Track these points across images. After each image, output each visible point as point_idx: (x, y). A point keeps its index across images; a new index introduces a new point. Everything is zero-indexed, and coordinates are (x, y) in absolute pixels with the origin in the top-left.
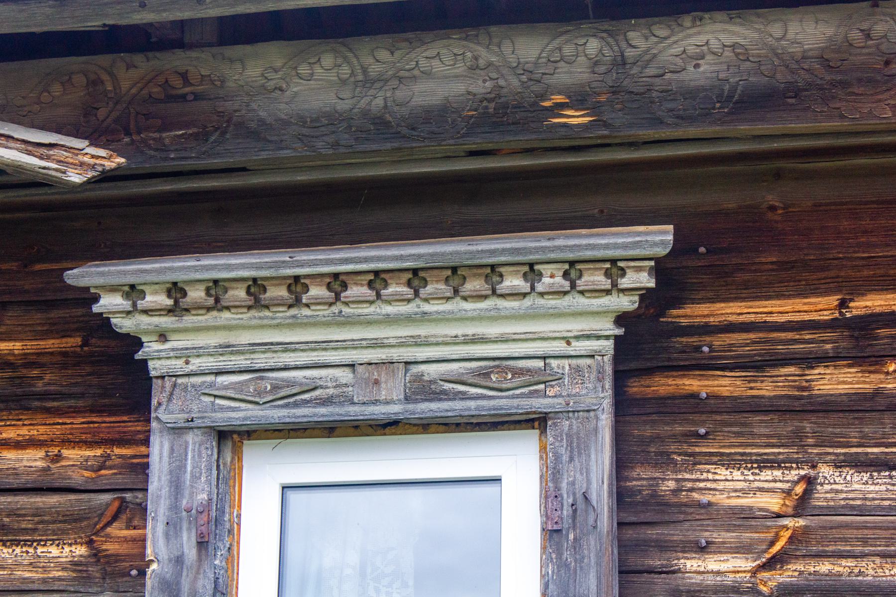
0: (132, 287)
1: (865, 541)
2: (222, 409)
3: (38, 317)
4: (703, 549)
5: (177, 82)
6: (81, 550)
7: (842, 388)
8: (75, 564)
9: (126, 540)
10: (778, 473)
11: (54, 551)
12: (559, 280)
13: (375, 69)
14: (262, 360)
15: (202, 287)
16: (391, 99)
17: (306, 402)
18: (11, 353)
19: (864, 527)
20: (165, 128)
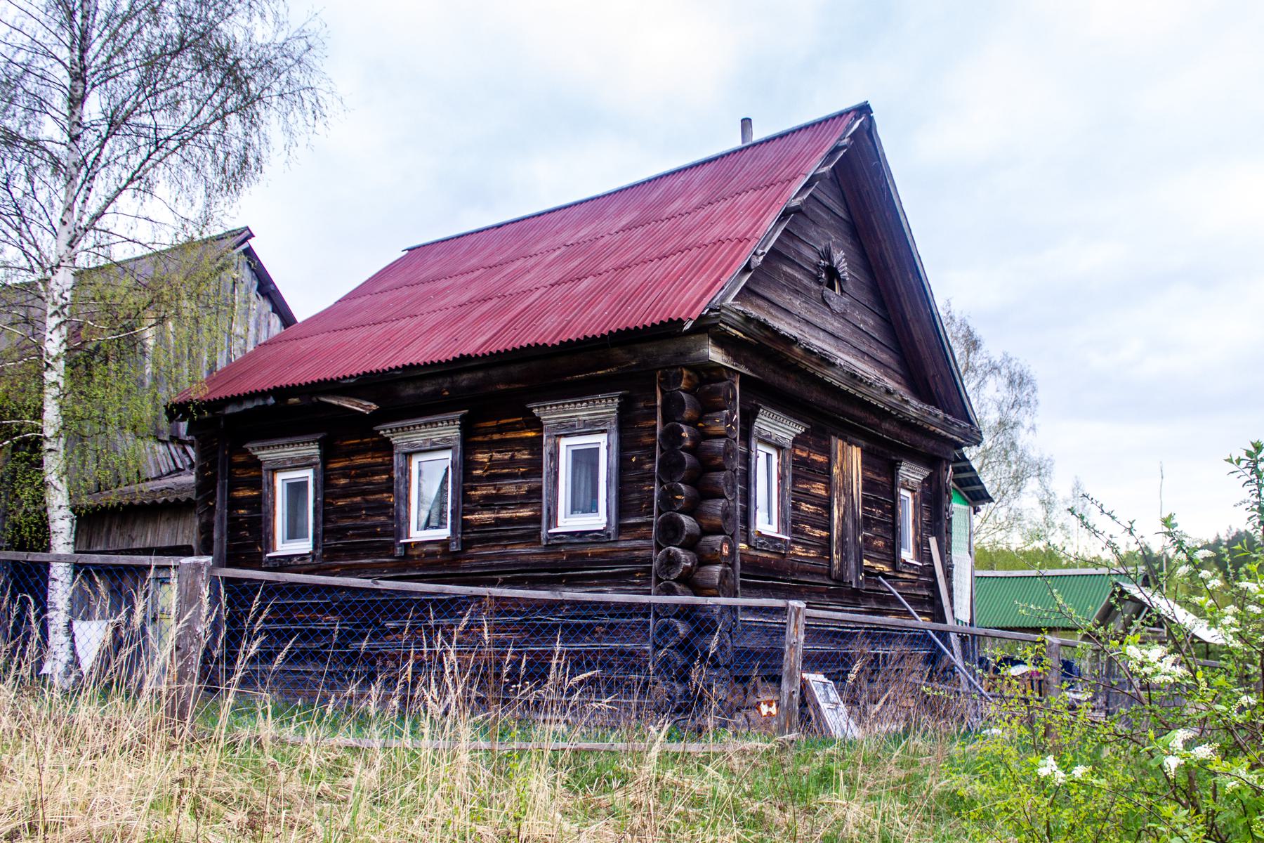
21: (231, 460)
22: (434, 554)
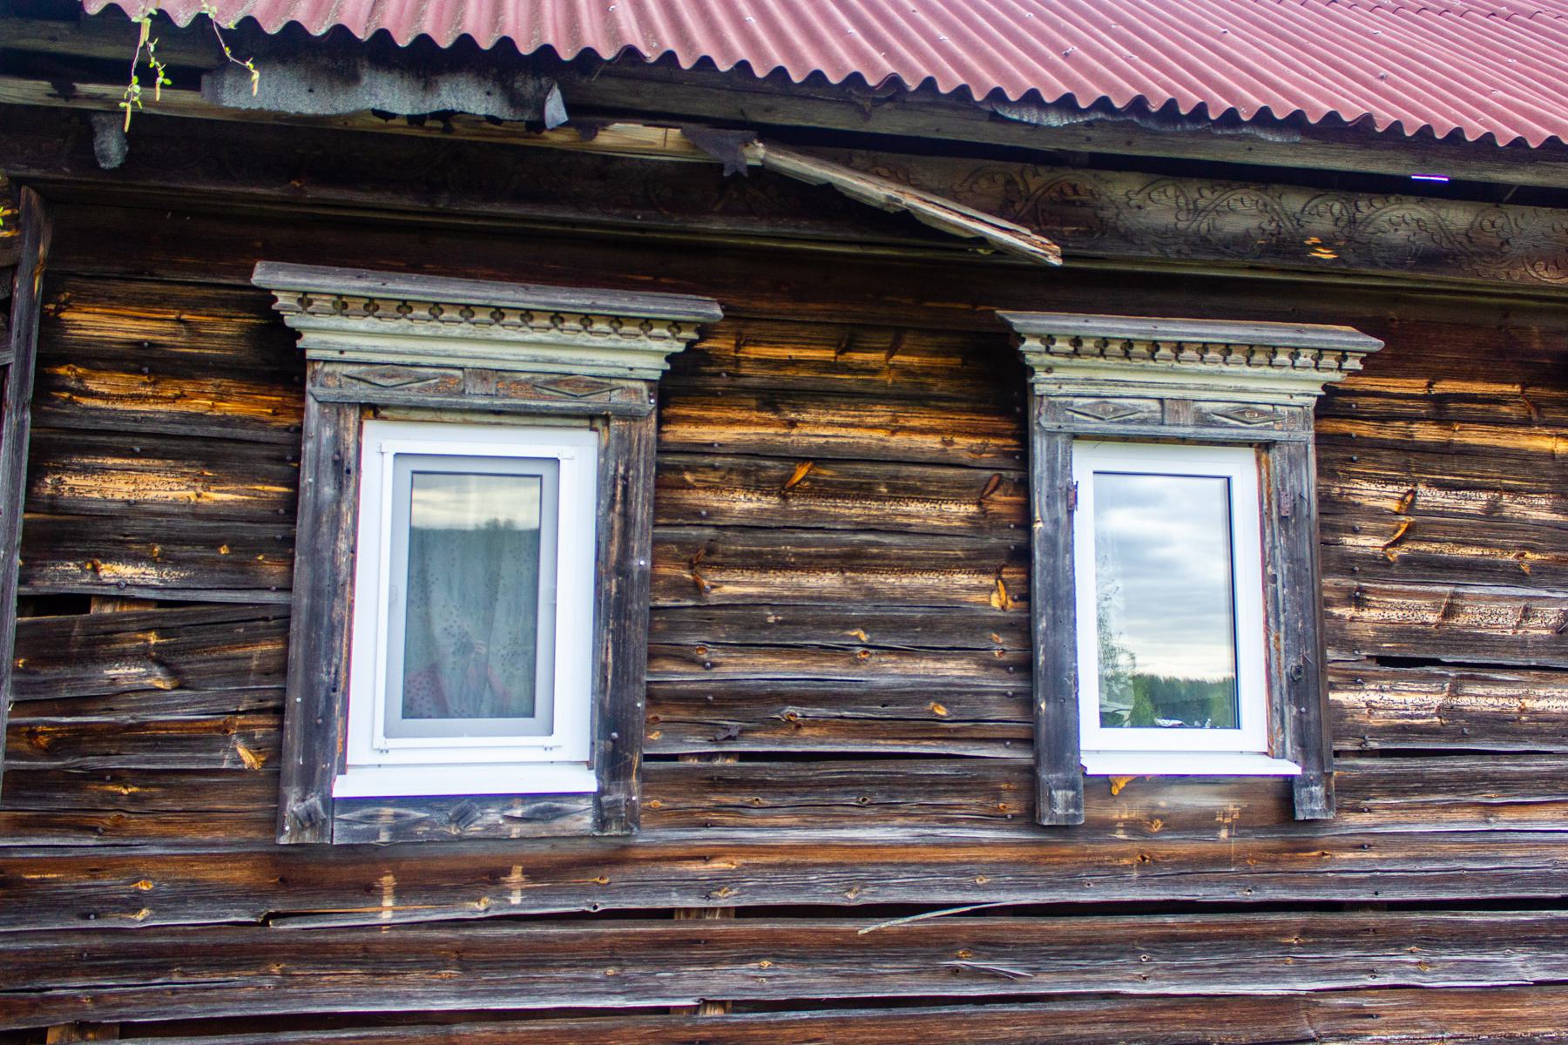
0: (1049, 336)
1: (1445, 533)
2: (1079, 421)
3: (928, 340)
4: (1355, 532)
5: (1069, 191)
6: (973, 509)
7: (1430, 438)
8: (969, 518)
9: (1005, 503)
10: (1396, 487)
11: (954, 508)
12: (1309, 359)
13: (1202, 203)
14: (1107, 391)
15: (1120, 343)
16: (1182, 216)
17: (1131, 421)
18: (911, 364)
19: (1445, 524)
20: (1063, 223)
21: (51, 325)
22: (1203, 823)
